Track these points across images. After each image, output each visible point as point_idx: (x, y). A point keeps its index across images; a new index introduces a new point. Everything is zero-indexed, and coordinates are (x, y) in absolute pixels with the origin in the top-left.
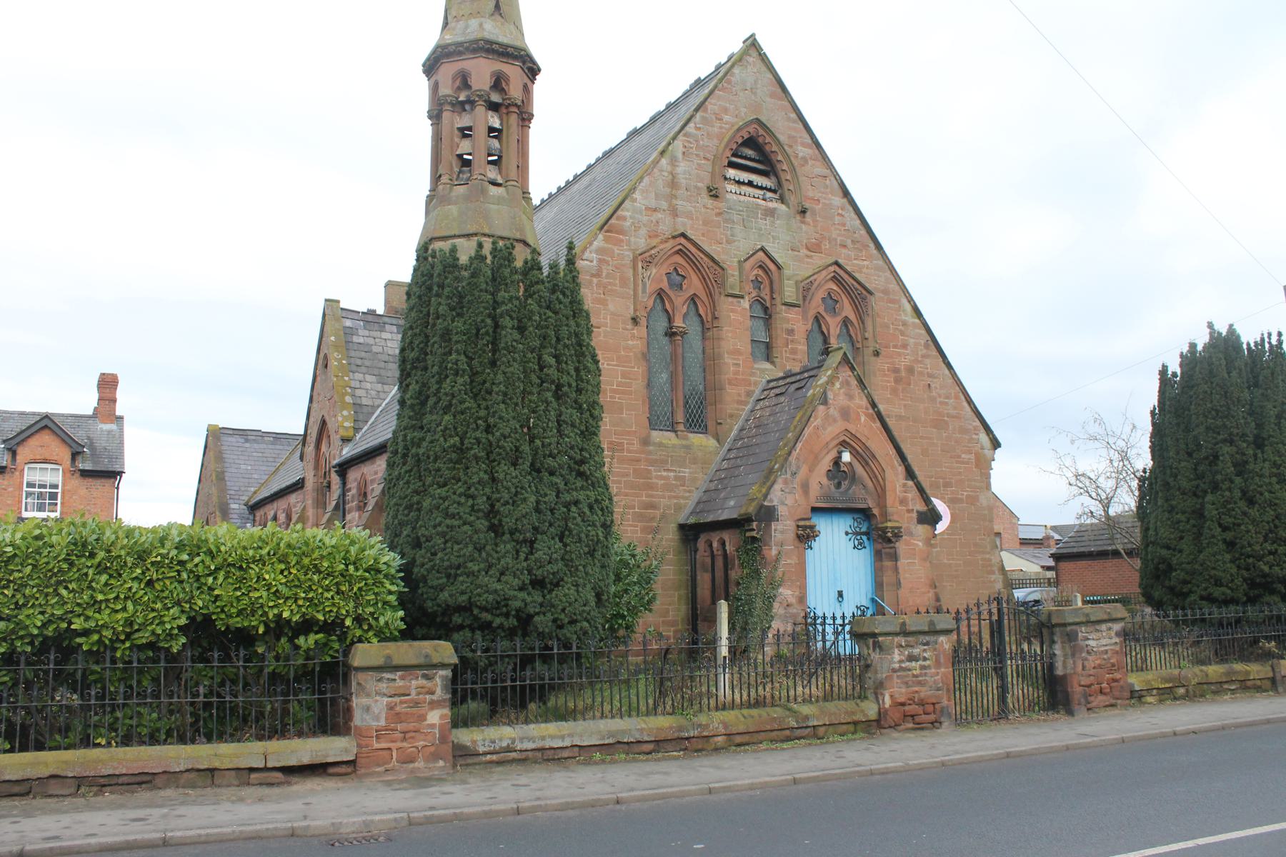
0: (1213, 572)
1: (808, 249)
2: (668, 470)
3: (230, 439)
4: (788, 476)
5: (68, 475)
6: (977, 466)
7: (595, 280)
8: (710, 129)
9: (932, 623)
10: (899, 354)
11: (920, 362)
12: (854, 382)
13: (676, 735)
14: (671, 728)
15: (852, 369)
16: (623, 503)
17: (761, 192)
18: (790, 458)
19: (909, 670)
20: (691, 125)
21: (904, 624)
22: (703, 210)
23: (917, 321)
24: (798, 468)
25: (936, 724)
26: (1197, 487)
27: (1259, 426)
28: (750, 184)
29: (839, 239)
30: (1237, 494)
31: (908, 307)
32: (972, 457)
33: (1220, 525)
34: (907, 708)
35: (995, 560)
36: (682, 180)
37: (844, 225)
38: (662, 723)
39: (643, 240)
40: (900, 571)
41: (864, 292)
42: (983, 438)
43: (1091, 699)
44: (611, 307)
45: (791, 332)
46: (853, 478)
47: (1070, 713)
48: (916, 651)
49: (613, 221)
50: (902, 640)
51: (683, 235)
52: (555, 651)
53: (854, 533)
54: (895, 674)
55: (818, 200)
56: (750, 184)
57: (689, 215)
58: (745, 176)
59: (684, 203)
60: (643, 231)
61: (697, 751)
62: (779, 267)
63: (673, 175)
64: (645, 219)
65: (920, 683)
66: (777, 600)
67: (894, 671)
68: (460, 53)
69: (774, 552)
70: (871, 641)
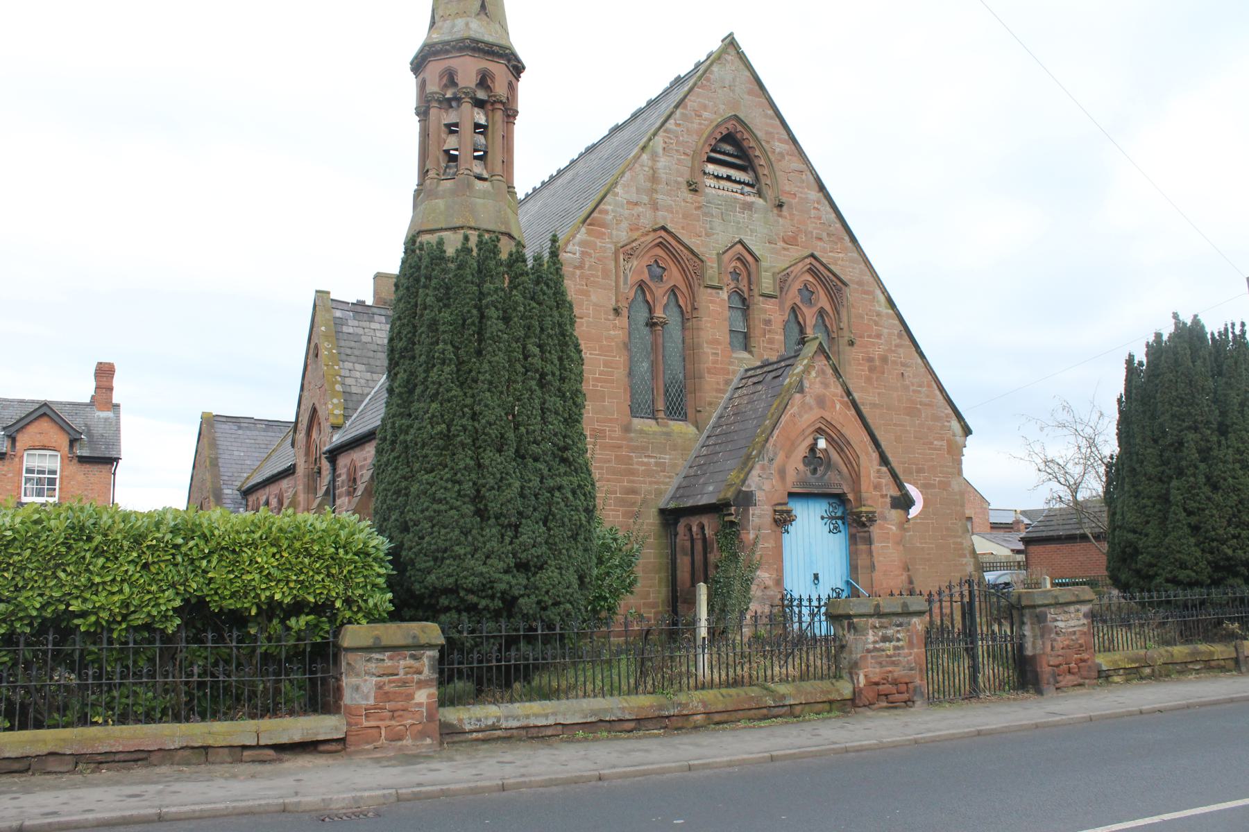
0: (1178, 556)
1: (784, 241)
2: (649, 456)
3: (223, 426)
4: (766, 462)
5: (66, 461)
6: (949, 452)
7: (578, 272)
8: (690, 125)
9: (905, 605)
10: (873, 344)
11: (894, 352)
12: (830, 371)
13: (657, 714)
14: (652, 707)
15: (828, 358)
16: (605, 488)
17: (740, 187)
18: (768, 445)
19: (883, 650)
20: (671, 121)
21: (878, 606)
22: (683, 204)
23: (891, 311)
24: (775, 454)
25: (909, 703)
26: (1163, 472)
27: (1223, 414)
28: (729, 178)
29: (815, 232)
30: (1202, 479)
31: (882, 298)
32: (944, 443)
33: (1185, 510)
34: (881, 687)
35: (966, 544)
36: (662, 175)
37: (820, 218)
38: (643, 702)
40: (874, 554)
41: (839, 283)
42: (955, 425)
44: (593, 298)
45: (768, 322)
46: (829, 464)
47: (1039, 692)
48: (890, 632)
49: (595, 215)
50: (876, 622)
51: (664, 228)
52: (539, 632)
53: (829, 518)
54: (869, 655)
55: (795, 194)
56: (729, 178)
57: (669, 209)
58: (723, 171)
59: (665, 197)
60: (625, 225)
61: (677, 729)
62: (756, 260)
63: (654, 170)
64: (626, 212)
65: (893, 663)
66: (755, 582)
67: (868, 651)
68: (447, 52)
69: (752, 536)
70: (846, 622)
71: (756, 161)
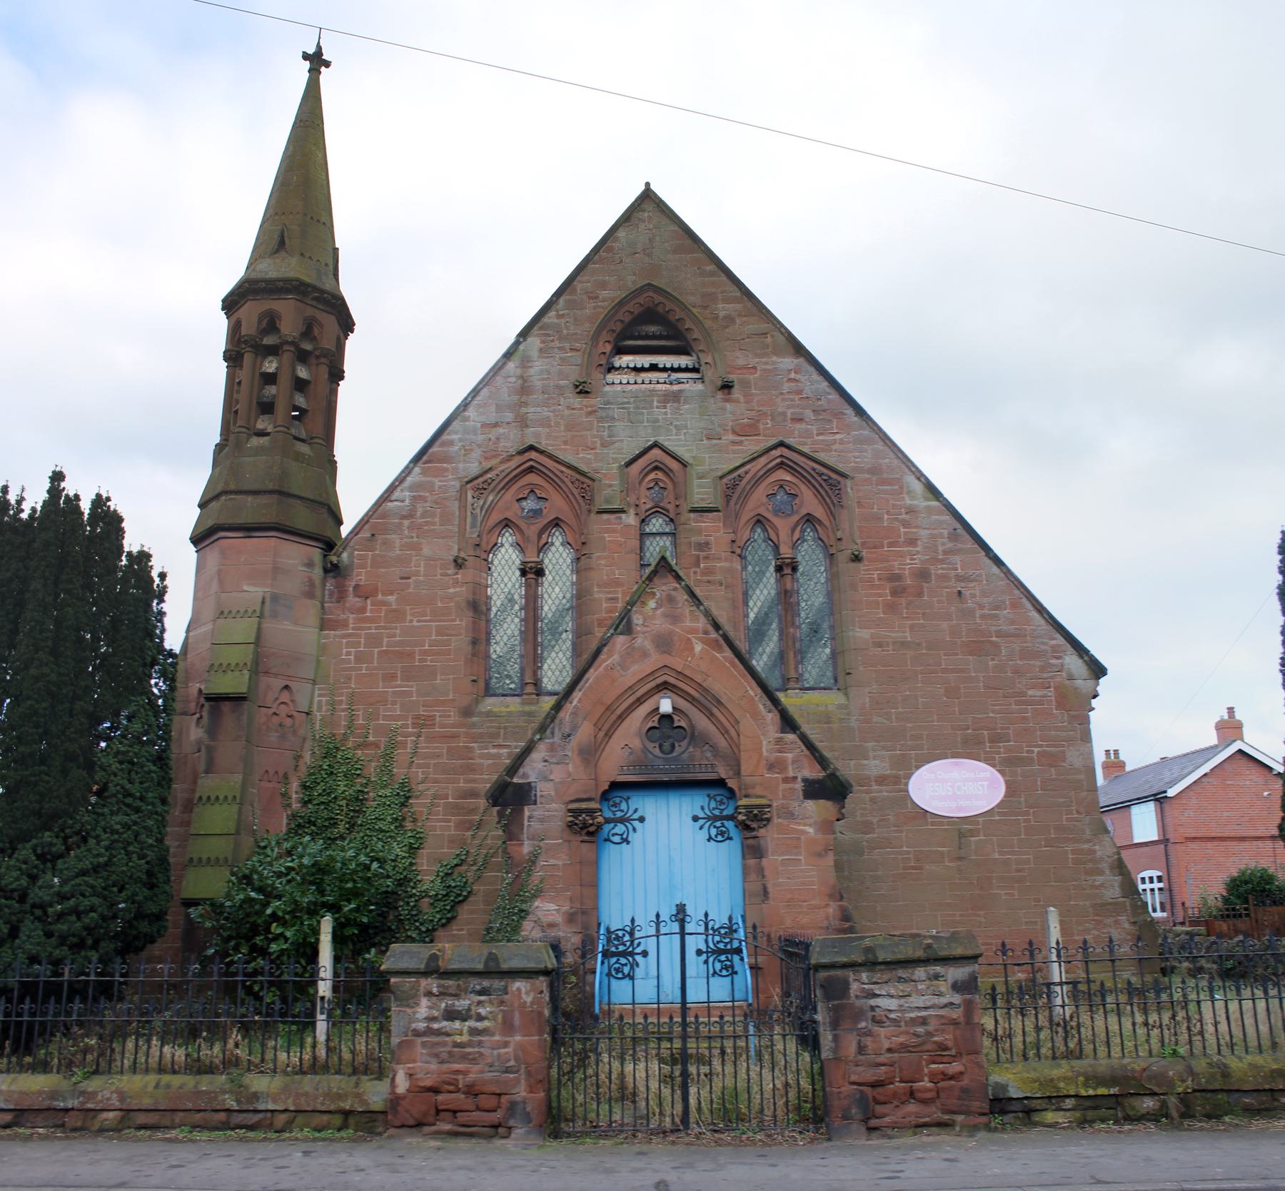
1: (734, 432)
2: (500, 746)
4: (557, 739)
6: (1060, 705)
7: (406, 523)
8: (578, 312)
9: (492, 958)
10: (902, 555)
11: (942, 561)
12: (683, 597)
13: (46, 1104)
14: (40, 1093)
15: (678, 578)
16: (432, 791)
17: (665, 375)
18: (561, 714)
19: (448, 1035)
20: (552, 313)
21: (434, 958)
22: (567, 412)
23: (935, 503)
24: (575, 728)
25: (497, 1130)
28: (654, 368)
29: (789, 412)
31: (918, 487)
32: (1051, 693)
34: (440, 1097)
35: (1104, 850)
36: (537, 383)
37: (800, 392)
40: (767, 873)
41: (833, 476)
42: (1073, 663)
43: (880, 1109)
44: (426, 551)
45: (704, 546)
46: (694, 737)
48: (462, 1004)
49: (435, 449)
50: (433, 984)
52: (66, 978)
53: (708, 818)
54: (419, 1040)
55: (754, 368)
56: (654, 368)
57: (545, 423)
58: (645, 360)
59: (539, 409)
60: (477, 454)
61: (75, 1130)
62: (684, 464)
64: (480, 438)
65: (464, 1058)
66: (530, 917)
67: (417, 1033)
69: (527, 848)
71: (688, 336)
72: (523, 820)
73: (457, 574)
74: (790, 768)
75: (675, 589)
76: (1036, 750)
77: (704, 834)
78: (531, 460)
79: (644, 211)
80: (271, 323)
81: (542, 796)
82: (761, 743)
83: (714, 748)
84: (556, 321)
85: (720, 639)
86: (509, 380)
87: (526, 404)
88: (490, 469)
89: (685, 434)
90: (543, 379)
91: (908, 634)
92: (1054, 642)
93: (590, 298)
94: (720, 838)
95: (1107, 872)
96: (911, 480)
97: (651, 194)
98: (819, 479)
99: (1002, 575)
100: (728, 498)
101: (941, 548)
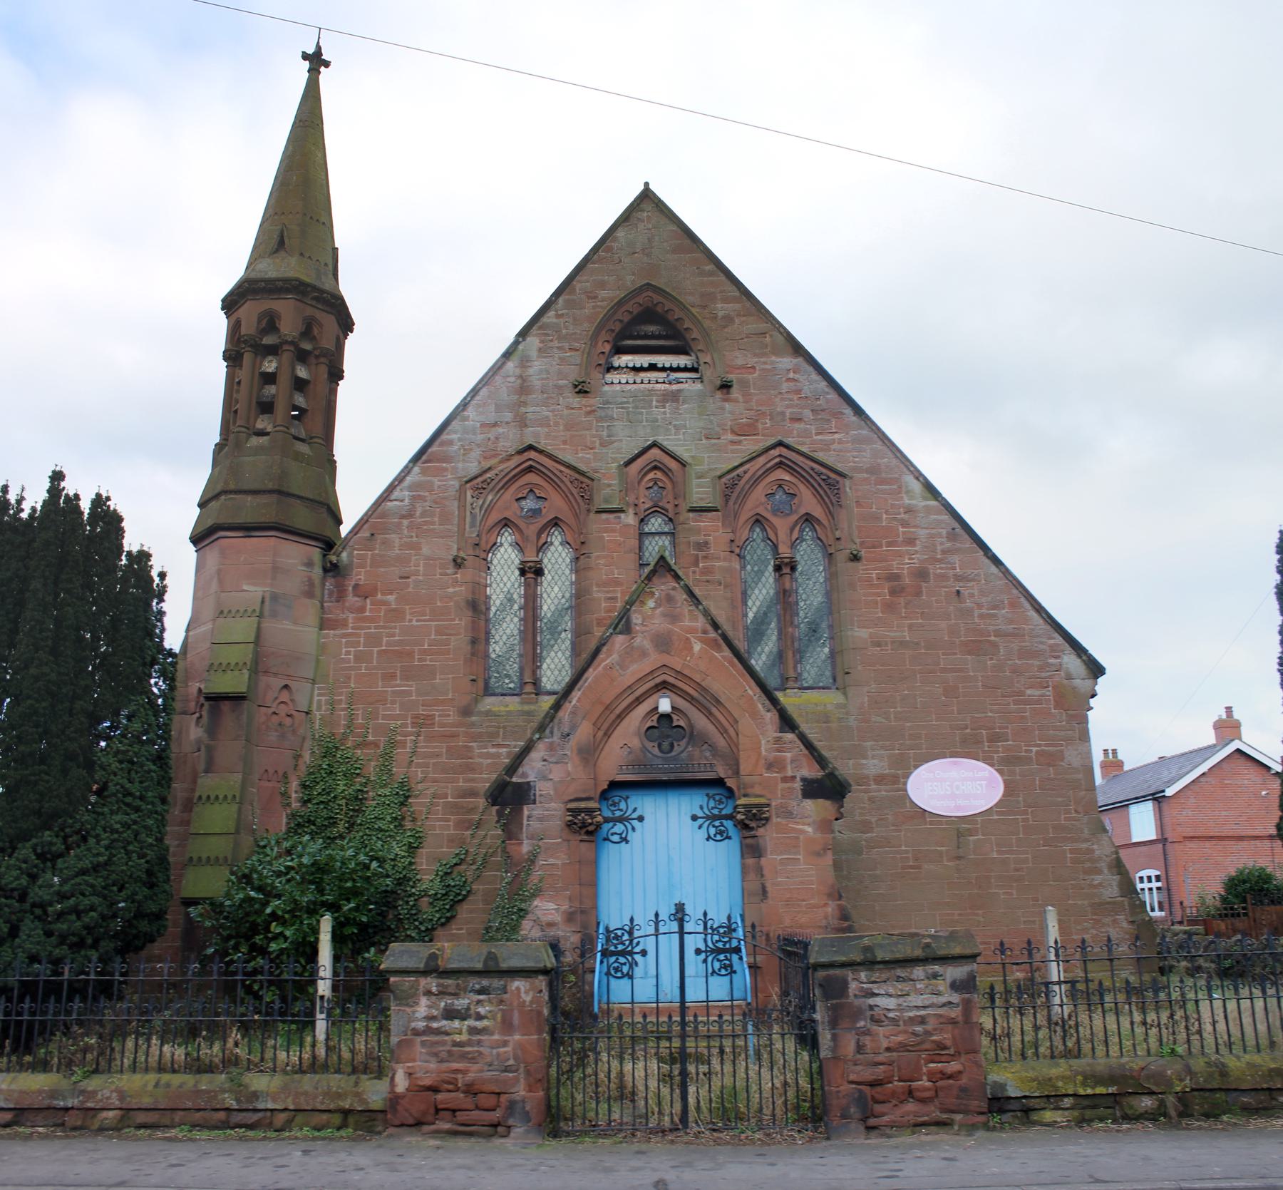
1: (733, 432)
2: (499, 746)
4: (556, 739)
6: (1058, 705)
7: (405, 522)
8: (578, 312)
9: (491, 957)
10: (900, 555)
11: (941, 561)
12: (682, 596)
13: (46, 1103)
14: (40, 1092)
15: (677, 577)
16: (431, 791)
17: (664, 375)
18: (560, 714)
19: (447, 1034)
20: (552, 313)
21: (433, 957)
22: (566, 412)
23: (934, 503)
24: (574, 727)
25: (496, 1129)
28: (653, 367)
29: (788, 412)
31: (916, 486)
32: (1049, 692)
34: (440, 1097)
36: (536, 383)
37: (798, 392)
39: (476, 464)
40: (765, 872)
41: (832, 475)
42: (1071, 662)
44: (426, 550)
45: (703, 545)
46: (693, 736)
48: (461, 1003)
49: (434, 449)
50: (432, 983)
52: (66, 977)
53: (707, 818)
54: (419, 1039)
55: (753, 367)
56: (653, 367)
57: (544, 422)
58: (644, 360)
59: (538, 409)
60: (476, 453)
61: (75, 1129)
62: (683, 464)
64: (480, 437)
65: (464, 1057)
66: (530, 916)
67: (416, 1033)
69: (526, 847)
71: (687, 336)
72: (522, 819)
73: (456, 573)
74: (789, 767)
75: (674, 589)
76: (1034, 749)
77: (703, 834)
78: (530, 459)
79: (643, 211)
80: (270, 323)
81: (541, 795)
82: (760, 742)
83: (713, 747)
84: (555, 320)
85: (719, 638)
86: (509, 379)
87: (525, 404)
88: (490, 469)
89: (684, 433)
90: (543, 379)
91: (906, 634)
92: (1052, 642)
93: (589, 298)
94: (719, 837)
95: (1106, 871)
96: (909, 479)
97: (650, 194)
98: (817, 478)
99: (1001, 575)
100: (727, 497)
101: (939, 548)
